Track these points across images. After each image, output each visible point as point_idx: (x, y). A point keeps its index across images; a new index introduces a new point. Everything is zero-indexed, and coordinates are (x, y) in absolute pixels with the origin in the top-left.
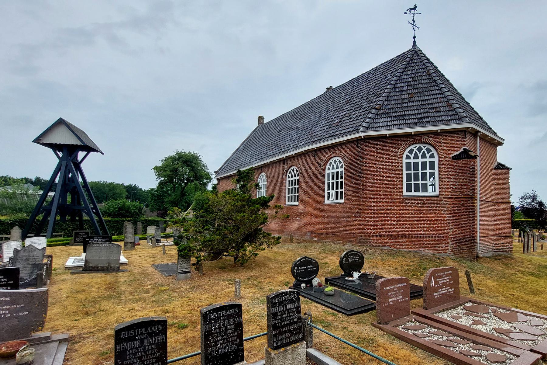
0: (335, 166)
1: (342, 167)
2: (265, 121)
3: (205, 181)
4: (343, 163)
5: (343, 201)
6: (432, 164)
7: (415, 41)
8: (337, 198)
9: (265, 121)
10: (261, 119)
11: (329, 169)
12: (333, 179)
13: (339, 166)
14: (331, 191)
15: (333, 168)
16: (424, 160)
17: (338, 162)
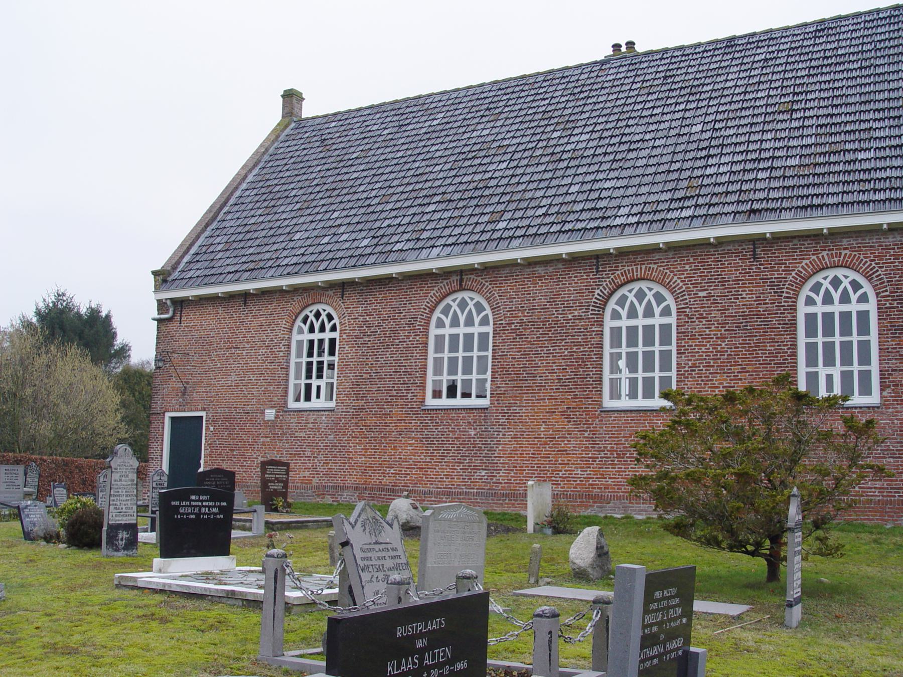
0: (462, 319)
1: (484, 322)
2: (308, 110)
3: (29, 391)
4: (488, 311)
5: (332, 404)
6: (863, 316)
8: (308, 398)
9: (308, 110)
10: (291, 98)
12: (310, 354)
13: (328, 327)
14: (315, 382)
17: (324, 316)
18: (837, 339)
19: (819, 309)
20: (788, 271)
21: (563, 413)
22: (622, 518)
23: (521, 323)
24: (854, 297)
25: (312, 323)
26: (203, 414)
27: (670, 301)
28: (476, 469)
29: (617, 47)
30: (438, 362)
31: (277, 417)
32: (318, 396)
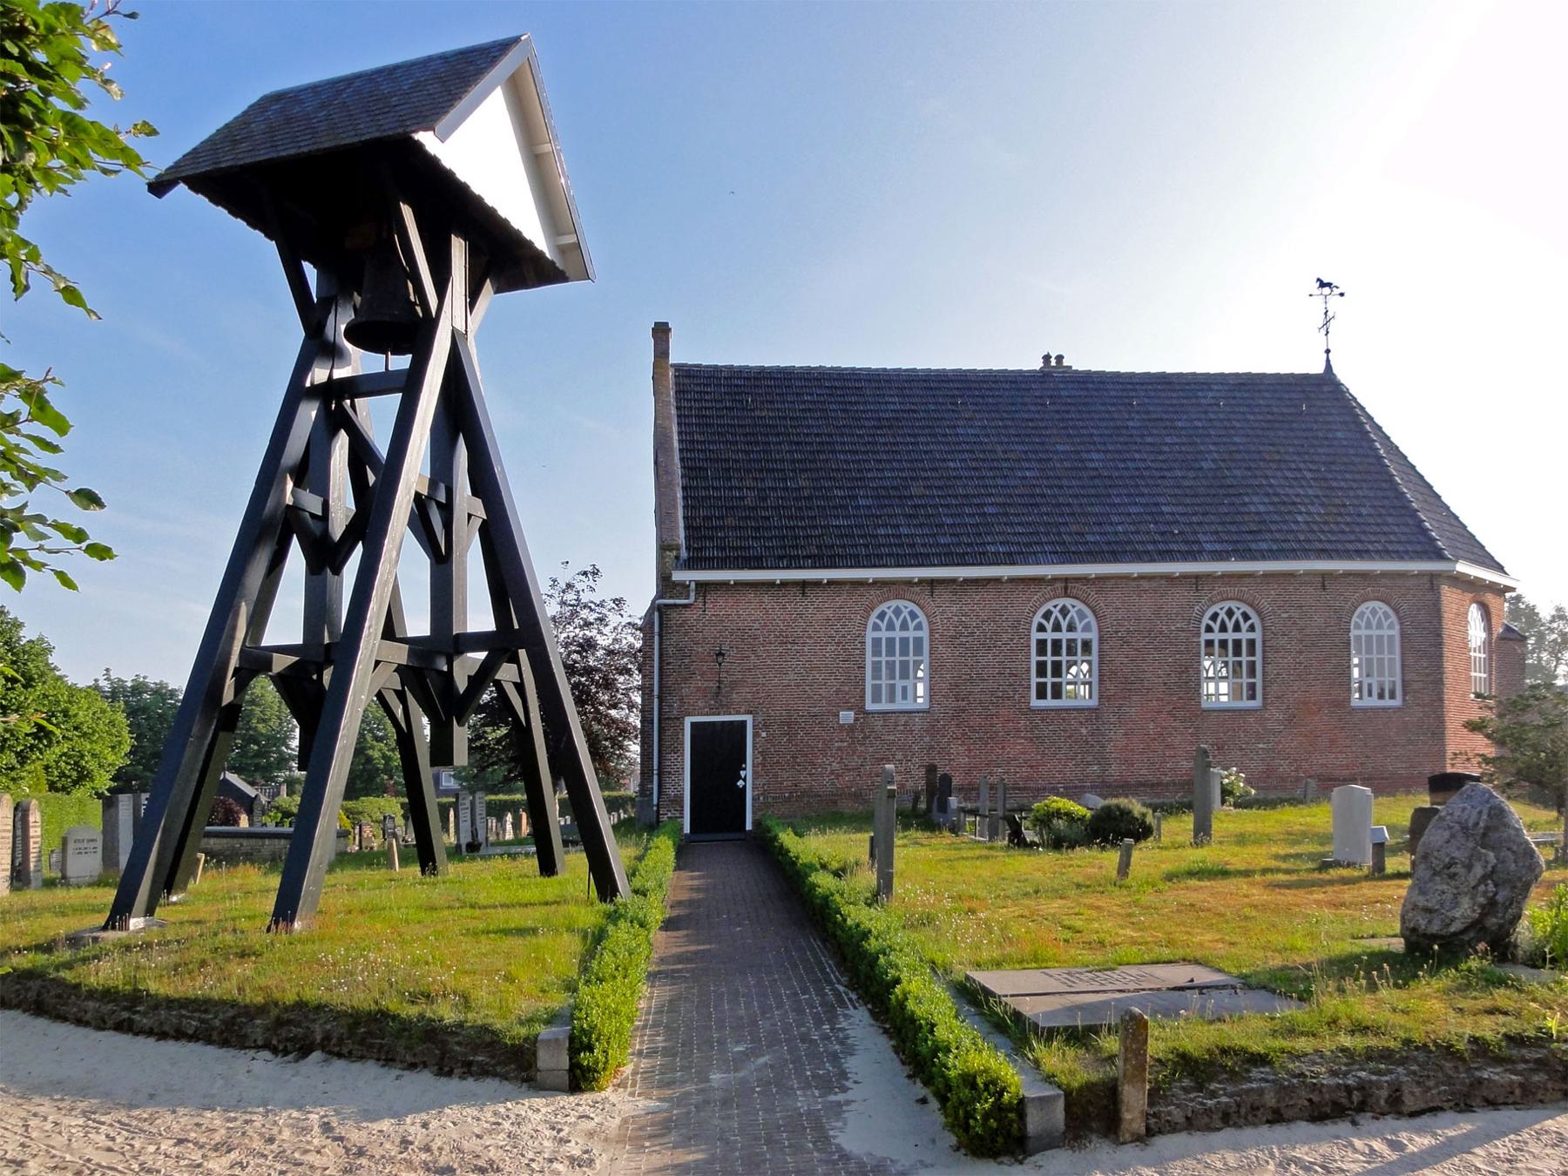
6: (918, 641)
7: (1328, 361)
8: (892, 699)
11: (1041, 628)
15: (1223, 628)
16: (905, 634)
18: (898, 658)
19: (884, 634)
20: (1346, 601)
21: (1169, 713)
22: (1354, 781)
23: (1128, 632)
24: (911, 625)
25: (1223, 622)
26: (749, 719)
27: (922, 618)
28: (1089, 764)
29: (1047, 358)
30: (877, 667)
31: (856, 719)
32: (1370, 694)
